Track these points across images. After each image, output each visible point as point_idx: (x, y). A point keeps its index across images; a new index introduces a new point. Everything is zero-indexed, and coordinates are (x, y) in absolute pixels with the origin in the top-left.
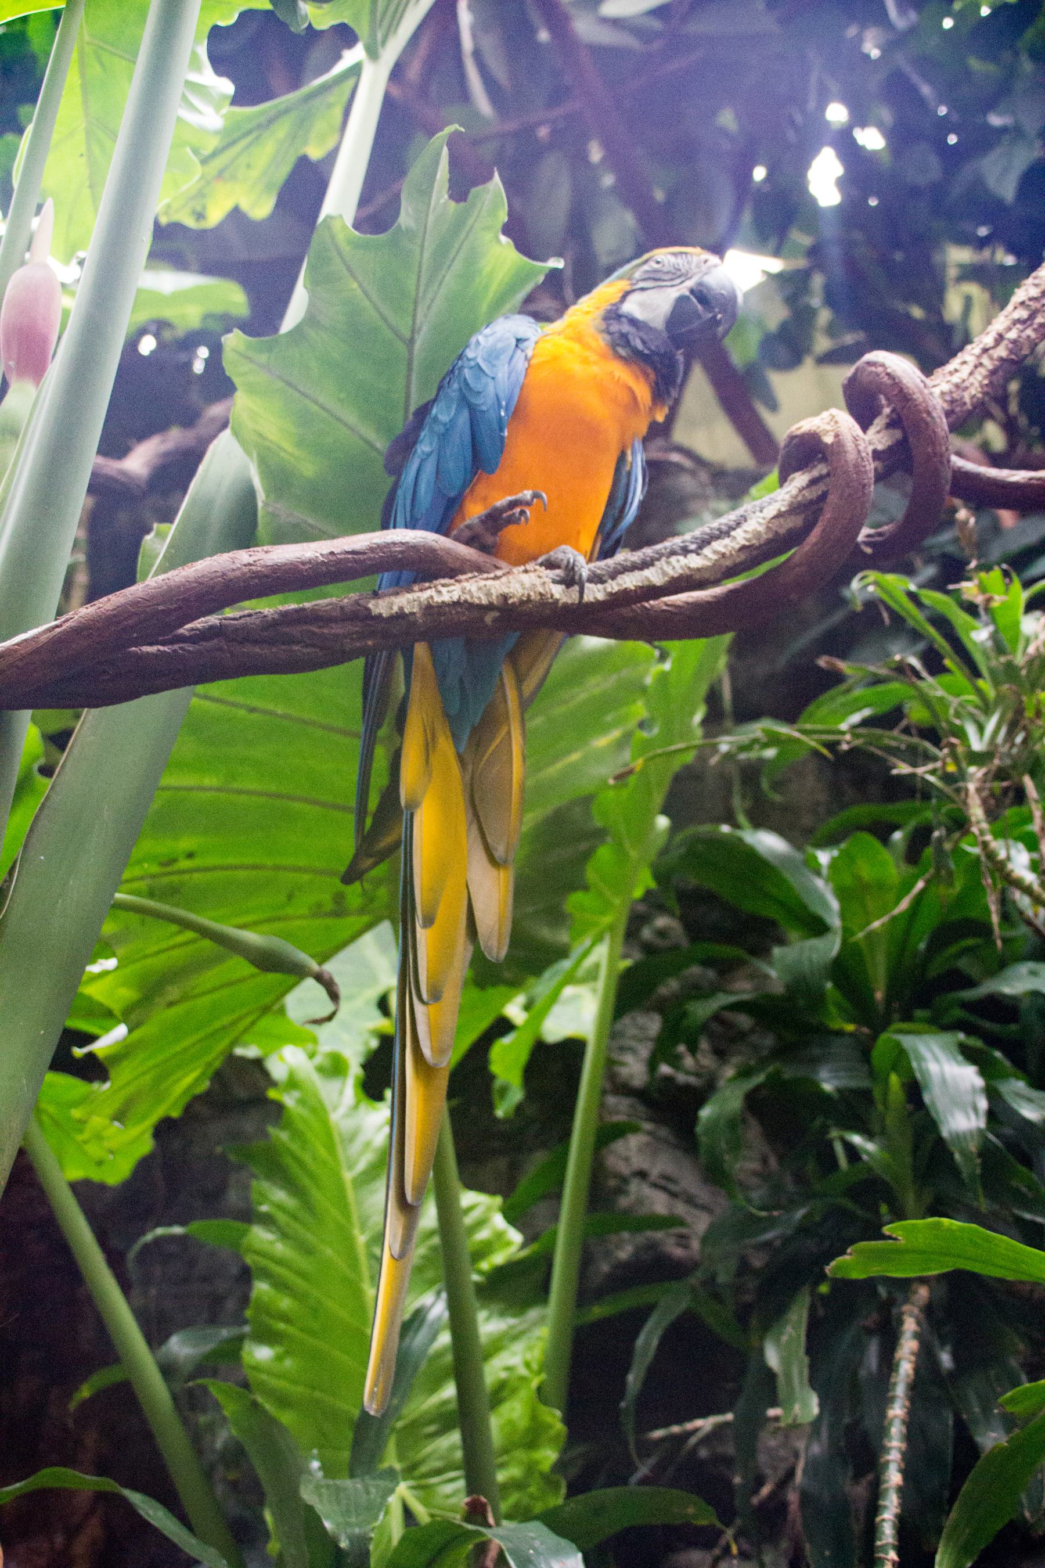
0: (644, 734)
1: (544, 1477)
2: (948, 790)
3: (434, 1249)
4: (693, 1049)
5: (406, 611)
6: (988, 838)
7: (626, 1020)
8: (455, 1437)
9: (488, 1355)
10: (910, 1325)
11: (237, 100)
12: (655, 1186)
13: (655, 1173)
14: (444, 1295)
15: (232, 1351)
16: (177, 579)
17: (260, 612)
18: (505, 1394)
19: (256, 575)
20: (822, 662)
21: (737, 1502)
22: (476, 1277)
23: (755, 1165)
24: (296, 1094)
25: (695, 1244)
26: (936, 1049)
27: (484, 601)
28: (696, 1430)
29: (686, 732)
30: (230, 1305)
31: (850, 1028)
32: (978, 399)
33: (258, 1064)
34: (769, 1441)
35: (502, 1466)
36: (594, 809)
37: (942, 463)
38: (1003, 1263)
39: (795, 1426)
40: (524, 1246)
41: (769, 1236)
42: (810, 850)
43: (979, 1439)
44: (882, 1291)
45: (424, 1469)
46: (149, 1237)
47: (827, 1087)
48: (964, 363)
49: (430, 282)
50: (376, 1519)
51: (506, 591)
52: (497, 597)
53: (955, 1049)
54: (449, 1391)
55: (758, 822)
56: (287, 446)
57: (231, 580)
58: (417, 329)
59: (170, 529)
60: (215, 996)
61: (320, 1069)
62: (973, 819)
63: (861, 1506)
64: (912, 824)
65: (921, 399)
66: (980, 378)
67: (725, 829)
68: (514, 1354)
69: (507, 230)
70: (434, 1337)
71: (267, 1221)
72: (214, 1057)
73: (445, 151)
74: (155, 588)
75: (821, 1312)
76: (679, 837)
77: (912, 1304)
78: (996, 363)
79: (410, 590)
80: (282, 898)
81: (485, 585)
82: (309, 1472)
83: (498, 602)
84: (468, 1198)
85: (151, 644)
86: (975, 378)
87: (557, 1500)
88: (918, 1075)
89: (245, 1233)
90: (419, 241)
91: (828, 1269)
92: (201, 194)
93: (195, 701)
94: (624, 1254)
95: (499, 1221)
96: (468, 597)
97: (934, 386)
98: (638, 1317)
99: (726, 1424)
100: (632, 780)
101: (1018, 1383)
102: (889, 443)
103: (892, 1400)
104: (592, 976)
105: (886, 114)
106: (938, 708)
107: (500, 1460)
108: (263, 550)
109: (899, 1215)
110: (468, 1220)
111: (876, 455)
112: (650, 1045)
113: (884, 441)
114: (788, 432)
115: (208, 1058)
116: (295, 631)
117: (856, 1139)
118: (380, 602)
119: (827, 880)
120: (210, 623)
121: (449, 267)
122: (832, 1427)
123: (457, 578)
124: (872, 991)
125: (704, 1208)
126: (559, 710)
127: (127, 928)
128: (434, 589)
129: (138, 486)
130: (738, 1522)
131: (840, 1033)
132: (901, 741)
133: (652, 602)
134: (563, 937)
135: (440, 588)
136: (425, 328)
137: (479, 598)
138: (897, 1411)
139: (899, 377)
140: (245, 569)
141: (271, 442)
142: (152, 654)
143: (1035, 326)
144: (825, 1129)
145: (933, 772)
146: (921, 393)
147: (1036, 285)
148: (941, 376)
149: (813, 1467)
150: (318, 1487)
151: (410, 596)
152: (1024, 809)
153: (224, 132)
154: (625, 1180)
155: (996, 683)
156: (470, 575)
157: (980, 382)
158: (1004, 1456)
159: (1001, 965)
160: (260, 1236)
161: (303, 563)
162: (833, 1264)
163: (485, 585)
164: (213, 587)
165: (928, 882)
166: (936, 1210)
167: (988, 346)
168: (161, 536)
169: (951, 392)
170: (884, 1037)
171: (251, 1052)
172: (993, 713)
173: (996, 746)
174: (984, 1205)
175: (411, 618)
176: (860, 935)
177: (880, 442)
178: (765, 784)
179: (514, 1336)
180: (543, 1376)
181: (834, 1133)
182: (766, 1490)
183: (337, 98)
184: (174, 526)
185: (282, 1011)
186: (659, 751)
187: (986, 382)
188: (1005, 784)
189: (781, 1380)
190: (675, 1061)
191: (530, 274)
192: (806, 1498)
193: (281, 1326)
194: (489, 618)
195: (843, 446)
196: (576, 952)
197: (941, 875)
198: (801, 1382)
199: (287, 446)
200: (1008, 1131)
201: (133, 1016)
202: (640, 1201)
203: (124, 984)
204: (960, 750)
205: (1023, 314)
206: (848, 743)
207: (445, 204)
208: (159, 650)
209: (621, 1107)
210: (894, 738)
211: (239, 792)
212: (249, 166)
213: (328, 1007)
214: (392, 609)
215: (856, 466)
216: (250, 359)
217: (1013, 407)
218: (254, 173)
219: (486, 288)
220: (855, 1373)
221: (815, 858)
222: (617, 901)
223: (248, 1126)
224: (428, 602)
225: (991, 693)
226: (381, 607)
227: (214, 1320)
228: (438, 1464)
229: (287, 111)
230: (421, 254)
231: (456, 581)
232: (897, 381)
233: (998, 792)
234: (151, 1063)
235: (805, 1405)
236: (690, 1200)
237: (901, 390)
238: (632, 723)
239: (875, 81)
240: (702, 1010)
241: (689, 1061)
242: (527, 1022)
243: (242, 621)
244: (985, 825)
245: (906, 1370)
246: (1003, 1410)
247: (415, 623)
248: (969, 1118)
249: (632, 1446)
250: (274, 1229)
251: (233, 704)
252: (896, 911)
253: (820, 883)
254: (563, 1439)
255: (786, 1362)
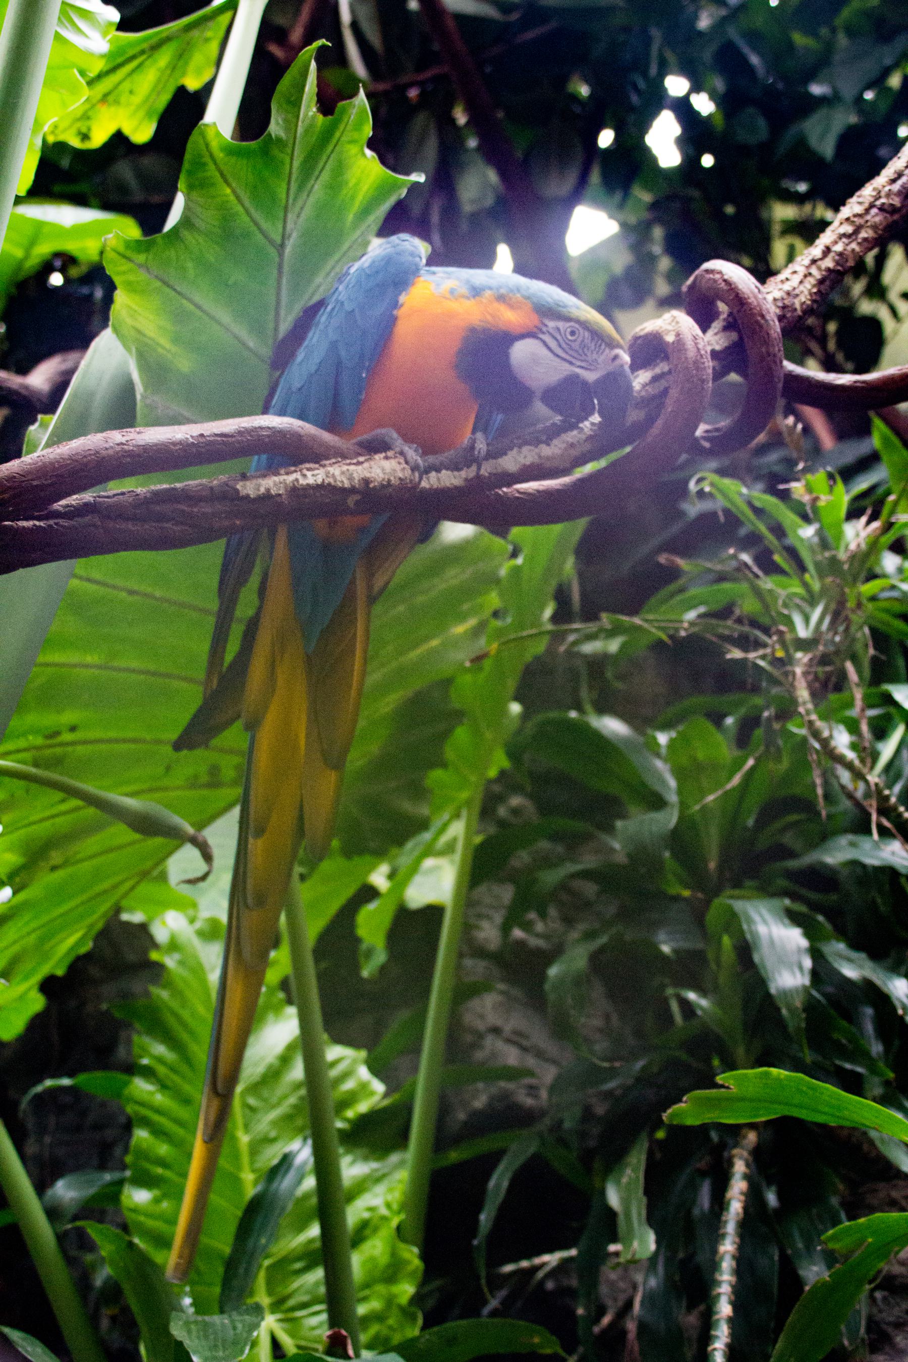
0: (497, 623)
1: (402, 1309)
2: (776, 673)
3: (302, 1098)
4: (543, 915)
5: (273, 492)
6: (814, 717)
7: (482, 889)
8: (319, 1274)
9: (351, 1197)
10: (740, 1167)
11: (122, 26)
12: (508, 1041)
13: (507, 1029)
14: (310, 1142)
15: (113, 1194)
16: (51, 456)
17: (133, 491)
18: (367, 1232)
19: (130, 454)
20: (662, 559)
21: (580, 1332)
22: (340, 1124)
23: (597, 1022)
24: (177, 956)
25: (544, 1094)
26: (764, 912)
27: (347, 484)
28: (543, 1265)
29: (536, 623)
30: (118, 1151)
31: (686, 893)
32: (808, 306)
33: (143, 928)
34: (609, 1273)
35: (364, 1299)
36: (453, 694)
37: (775, 362)
38: (826, 1109)
39: (634, 1262)
40: (386, 1095)
41: (611, 1085)
42: (649, 731)
43: (802, 1273)
44: (714, 1136)
45: (291, 1302)
46: (39, 1088)
47: (666, 949)
48: (795, 272)
49: (301, 188)
50: (242, 1352)
51: (368, 475)
52: (359, 481)
53: (782, 914)
54: (314, 1231)
55: (602, 709)
56: (164, 342)
57: (104, 458)
58: (287, 236)
59: (52, 419)
60: (95, 862)
61: (201, 934)
62: (800, 700)
63: (694, 1334)
64: (743, 711)
65: (755, 303)
66: (809, 287)
67: (573, 714)
68: (376, 1195)
69: (372, 144)
70: (299, 1181)
71: (148, 1073)
72: (97, 918)
73: (313, 65)
74: (30, 464)
75: (658, 1156)
76: (529, 724)
77: (742, 1148)
78: (824, 273)
79: (277, 474)
80: (161, 770)
81: (348, 470)
82: (181, 1310)
83: (359, 485)
84: (334, 1052)
85: (27, 519)
86: (805, 287)
87: (413, 1331)
88: (748, 937)
89: (127, 1084)
90: (289, 151)
91: (665, 1116)
92: (86, 117)
93: (74, 583)
94: (479, 1103)
95: (363, 1072)
96: (331, 480)
97: (768, 293)
98: (488, 1163)
99: (570, 1260)
100: (487, 664)
101: (840, 1222)
102: (726, 344)
103: (724, 1236)
104: (449, 849)
105: (719, 84)
106: (768, 599)
107: (362, 1294)
108: (135, 431)
109: (730, 1065)
110: (334, 1073)
111: (714, 354)
112: (503, 912)
113: (721, 342)
114: (632, 333)
115: (90, 920)
116: (166, 508)
117: (692, 996)
118: (248, 483)
119: (665, 760)
120: (84, 501)
121: (317, 178)
122: (669, 1261)
123: (322, 463)
124: (705, 862)
125: (554, 1062)
126: (421, 599)
127: (12, 796)
128: (299, 473)
129: (39, 400)
130: (581, 1349)
131: (676, 898)
132: (735, 630)
133: (505, 489)
134: (424, 810)
135: (305, 472)
136: (295, 235)
137: (342, 482)
138: (728, 1246)
139: (735, 283)
140: (118, 448)
141: (150, 338)
142: (28, 528)
143: (859, 240)
144: (663, 987)
145: (763, 657)
146: (756, 297)
147: (860, 203)
148: (774, 284)
149: (650, 1299)
150: (187, 1323)
151: (276, 479)
152: (844, 695)
153: (109, 56)
154: (481, 1036)
155: (821, 576)
156: (334, 460)
157: (810, 290)
158: (825, 1290)
159: (824, 837)
160: (141, 1087)
161: (174, 444)
162: (669, 1111)
163: (348, 470)
164: (86, 465)
165: (758, 760)
166: (765, 1059)
167: (816, 258)
168: (44, 426)
169: (783, 299)
170: (717, 902)
171: (135, 917)
172: (818, 604)
173: (821, 633)
174: (808, 1056)
175: (278, 499)
176: (697, 807)
177: (718, 343)
178: (609, 674)
179: (376, 1179)
180: (402, 1216)
181: (670, 991)
182: (606, 1320)
183: (214, 32)
184: (56, 417)
185: (163, 877)
186: (512, 636)
187: (815, 290)
188: (828, 669)
189: (621, 1219)
190: (527, 926)
191: (395, 186)
192: (643, 1327)
193: (159, 1171)
194: (351, 501)
195: (684, 344)
196: (436, 824)
197: (771, 751)
198: (640, 1221)
199: (164, 342)
200: (830, 989)
201: (17, 880)
202: (494, 1055)
203: (9, 849)
204: (788, 637)
205: (848, 229)
206: (685, 629)
207: (313, 117)
208: (35, 525)
209: (477, 968)
210: (728, 627)
211: (119, 670)
212: (131, 92)
213: (202, 867)
214: (259, 490)
215: (695, 362)
216: (129, 260)
217: (832, 345)
218: (137, 99)
219: (353, 198)
220: (689, 1212)
221: (655, 739)
222: (473, 779)
223: (136, 987)
224: (294, 484)
225: (816, 586)
226: (249, 488)
227: (103, 1166)
228: (305, 1298)
229: (168, 39)
230: (291, 163)
231: (321, 466)
232: (733, 286)
233: (821, 675)
234: (34, 925)
235: (643, 1242)
236: (540, 1054)
237: (737, 295)
238: (488, 612)
239: (707, 54)
240: (550, 878)
241: (540, 927)
242: (391, 891)
243: (115, 499)
244: (810, 706)
245: (736, 1209)
246: (825, 1246)
247: (280, 505)
248: (795, 977)
249: (483, 1281)
250: (153, 1080)
251: (114, 587)
252: (729, 786)
253: (659, 764)
254: (420, 1274)
255: (626, 1202)
